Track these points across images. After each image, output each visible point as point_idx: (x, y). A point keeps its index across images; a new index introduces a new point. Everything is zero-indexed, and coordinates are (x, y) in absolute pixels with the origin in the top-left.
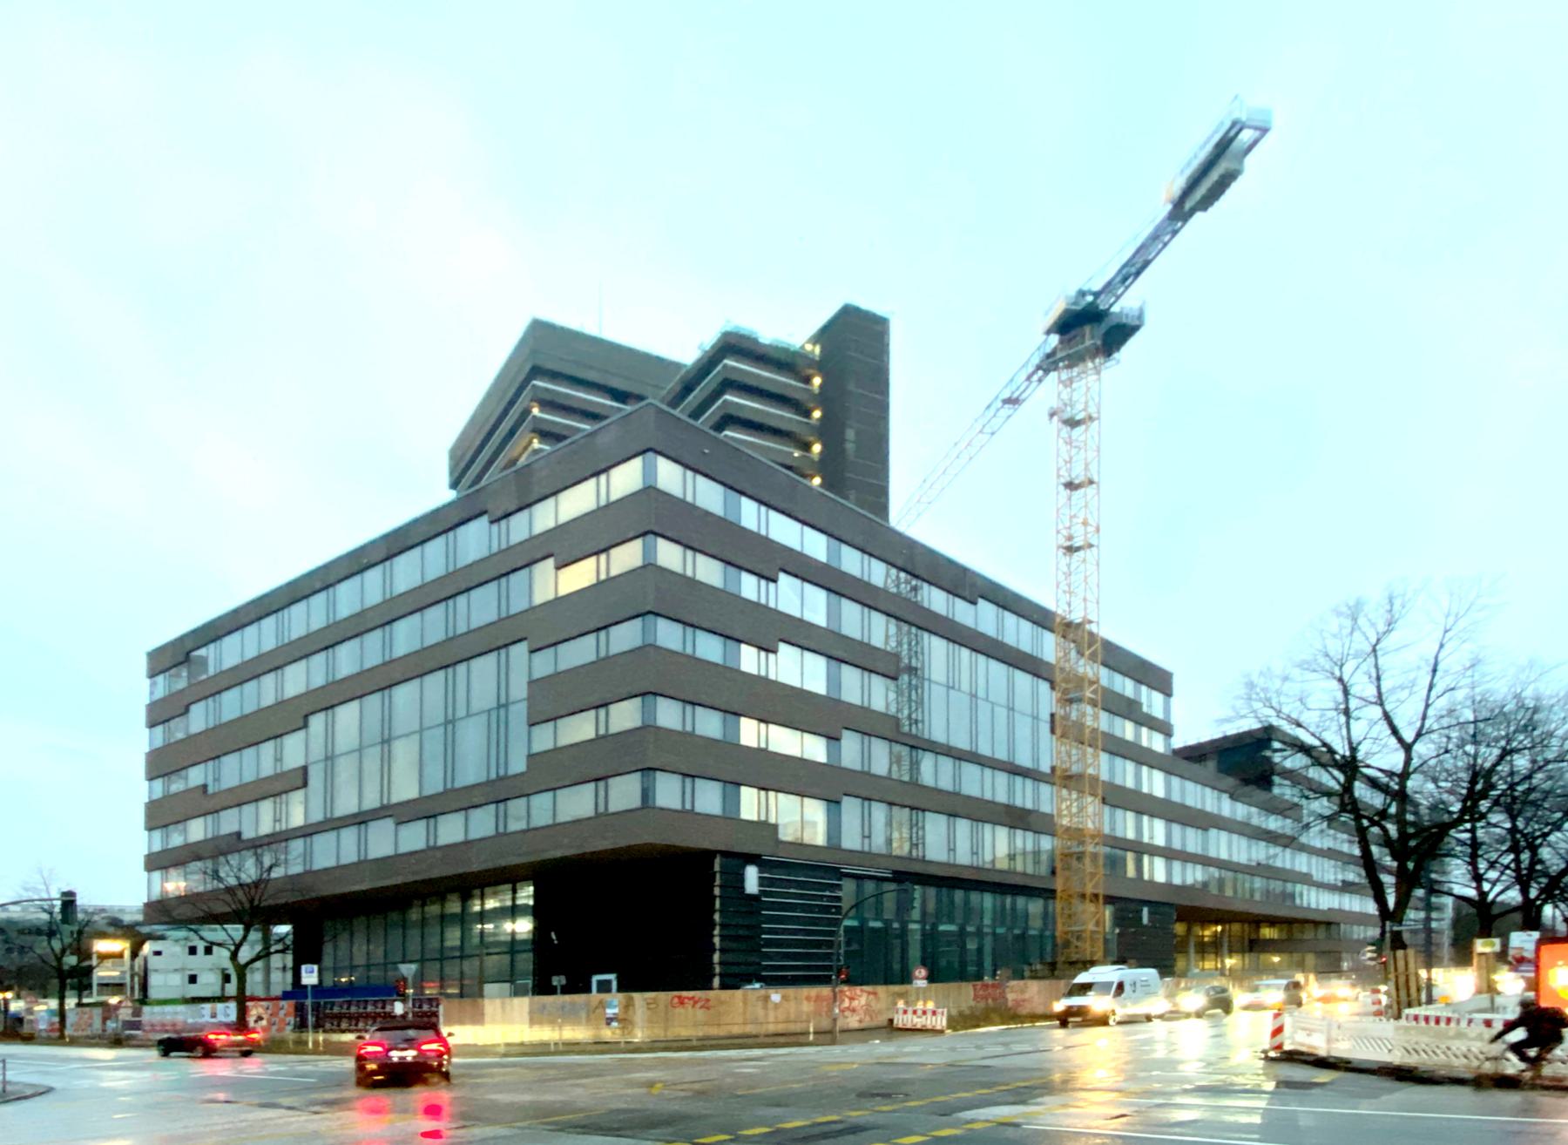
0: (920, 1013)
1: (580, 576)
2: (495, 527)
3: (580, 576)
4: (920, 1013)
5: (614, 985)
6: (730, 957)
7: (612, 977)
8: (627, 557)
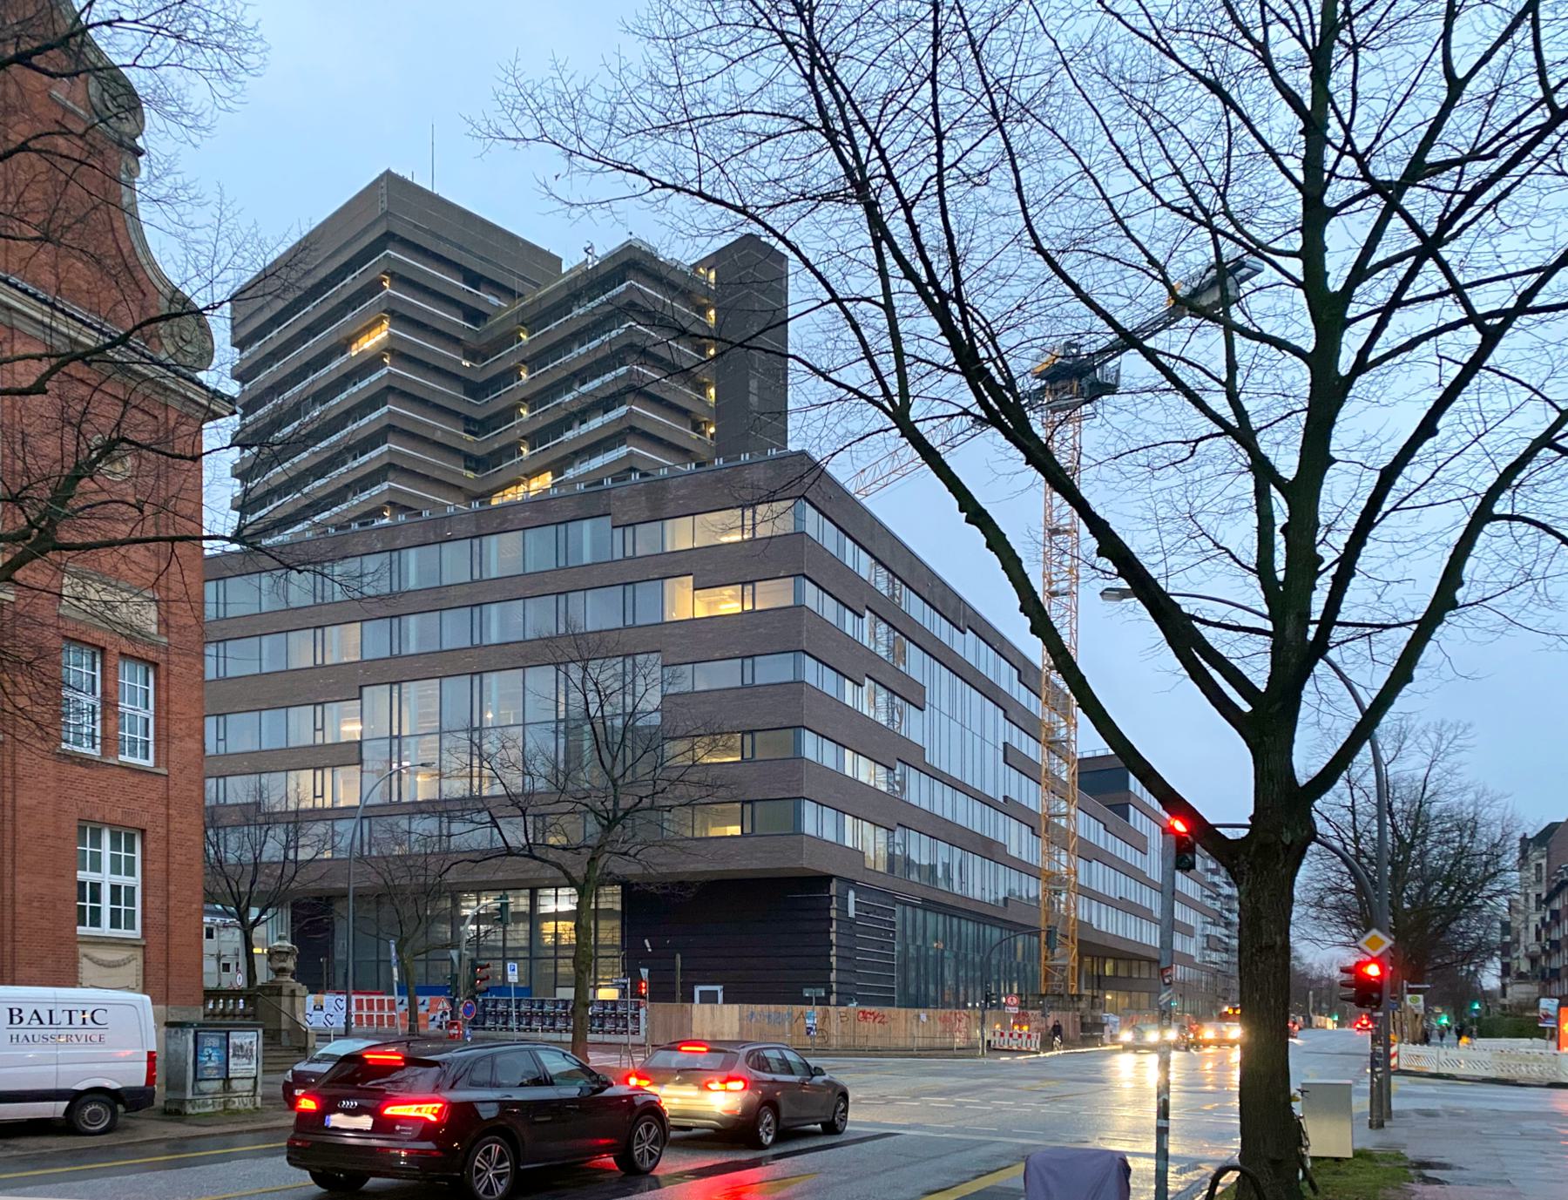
0: (1015, 1036)
1: (728, 602)
2: (618, 532)
3: (728, 602)
4: (1015, 1036)
5: (720, 996)
6: (844, 977)
7: (718, 988)
8: (773, 595)
